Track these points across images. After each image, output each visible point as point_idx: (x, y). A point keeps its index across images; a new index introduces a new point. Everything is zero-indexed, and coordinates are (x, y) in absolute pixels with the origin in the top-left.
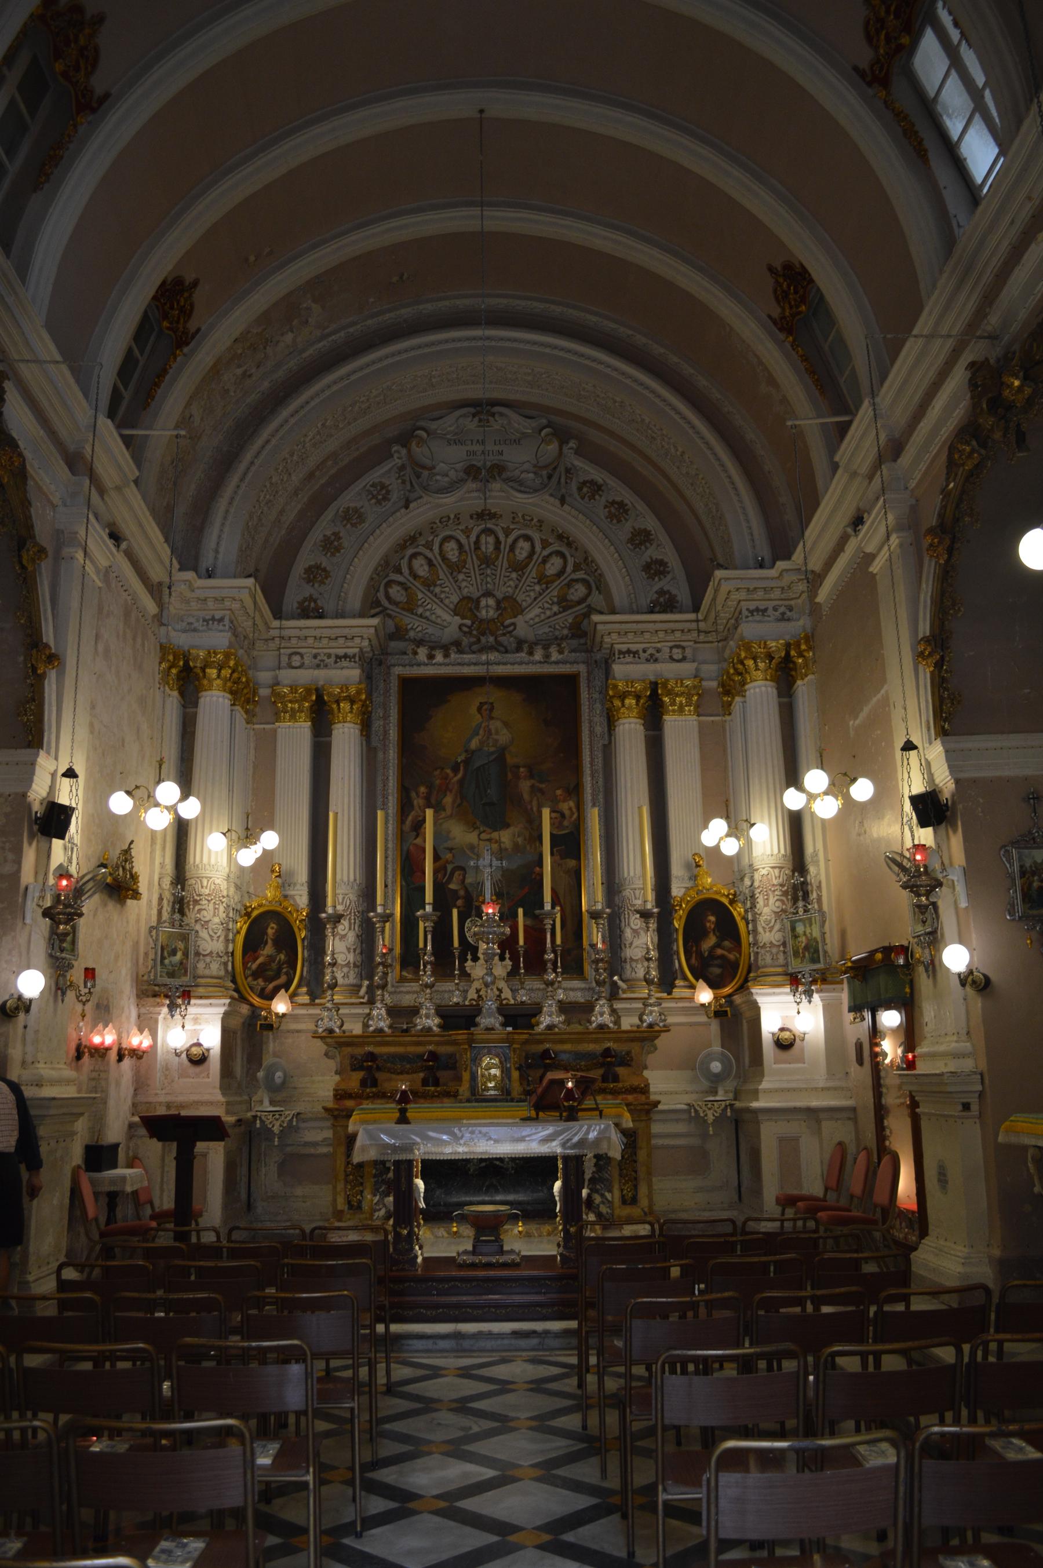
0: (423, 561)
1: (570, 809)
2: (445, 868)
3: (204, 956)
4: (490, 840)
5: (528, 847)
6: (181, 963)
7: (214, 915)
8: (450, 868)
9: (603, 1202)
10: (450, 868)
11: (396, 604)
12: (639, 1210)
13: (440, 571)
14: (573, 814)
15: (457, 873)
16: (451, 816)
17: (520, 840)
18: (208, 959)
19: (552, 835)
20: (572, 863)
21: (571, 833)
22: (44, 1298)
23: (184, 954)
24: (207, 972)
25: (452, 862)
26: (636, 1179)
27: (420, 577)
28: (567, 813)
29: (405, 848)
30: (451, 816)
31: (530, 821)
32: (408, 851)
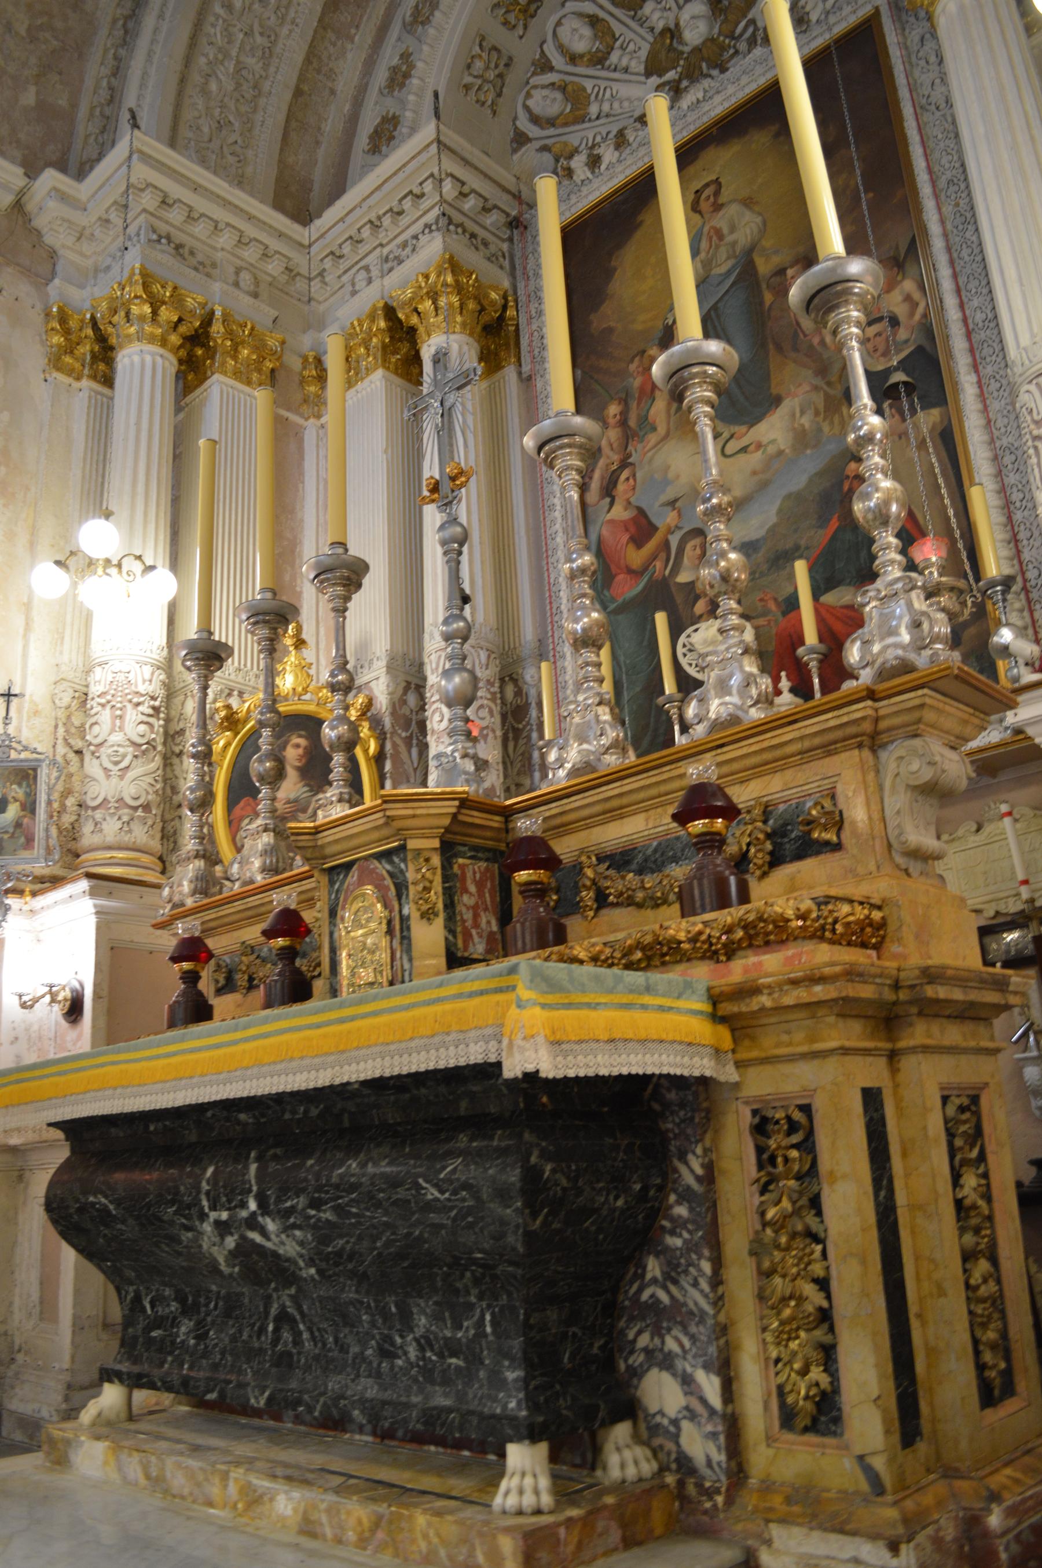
0: (576, 23)
1: (908, 298)
2: (666, 545)
3: (94, 808)
4: (744, 450)
5: (826, 428)
6: (18, 825)
7: (113, 731)
8: (674, 541)
9: (691, 1414)
10: (674, 541)
11: (551, 122)
12: (848, 1464)
13: (613, 23)
14: (914, 305)
15: (689, 546)
16: (666, 437)
17: (806, 421)
18: (98, 815)
19: (868, 373)
20: (928, 419)
21: (920, 350)
22: (663, 1343)
23: (23, 807)
24: (96, 839)
25: (678, 528)
26: (825, 1317)
27: (581, 56)
28: (901, 310)
29: (594, 537)
30: (666, 437)
31: (822, 371)
32: (600, 542)
